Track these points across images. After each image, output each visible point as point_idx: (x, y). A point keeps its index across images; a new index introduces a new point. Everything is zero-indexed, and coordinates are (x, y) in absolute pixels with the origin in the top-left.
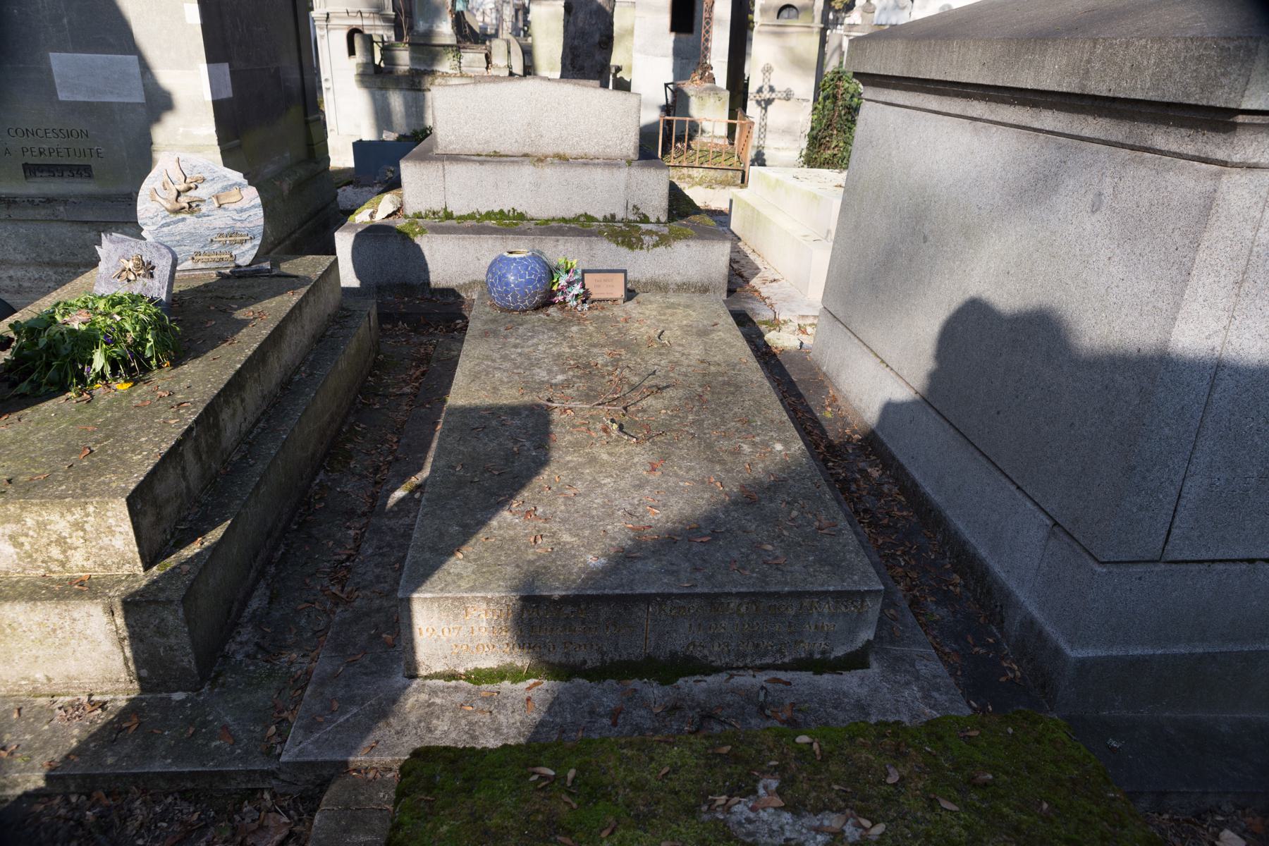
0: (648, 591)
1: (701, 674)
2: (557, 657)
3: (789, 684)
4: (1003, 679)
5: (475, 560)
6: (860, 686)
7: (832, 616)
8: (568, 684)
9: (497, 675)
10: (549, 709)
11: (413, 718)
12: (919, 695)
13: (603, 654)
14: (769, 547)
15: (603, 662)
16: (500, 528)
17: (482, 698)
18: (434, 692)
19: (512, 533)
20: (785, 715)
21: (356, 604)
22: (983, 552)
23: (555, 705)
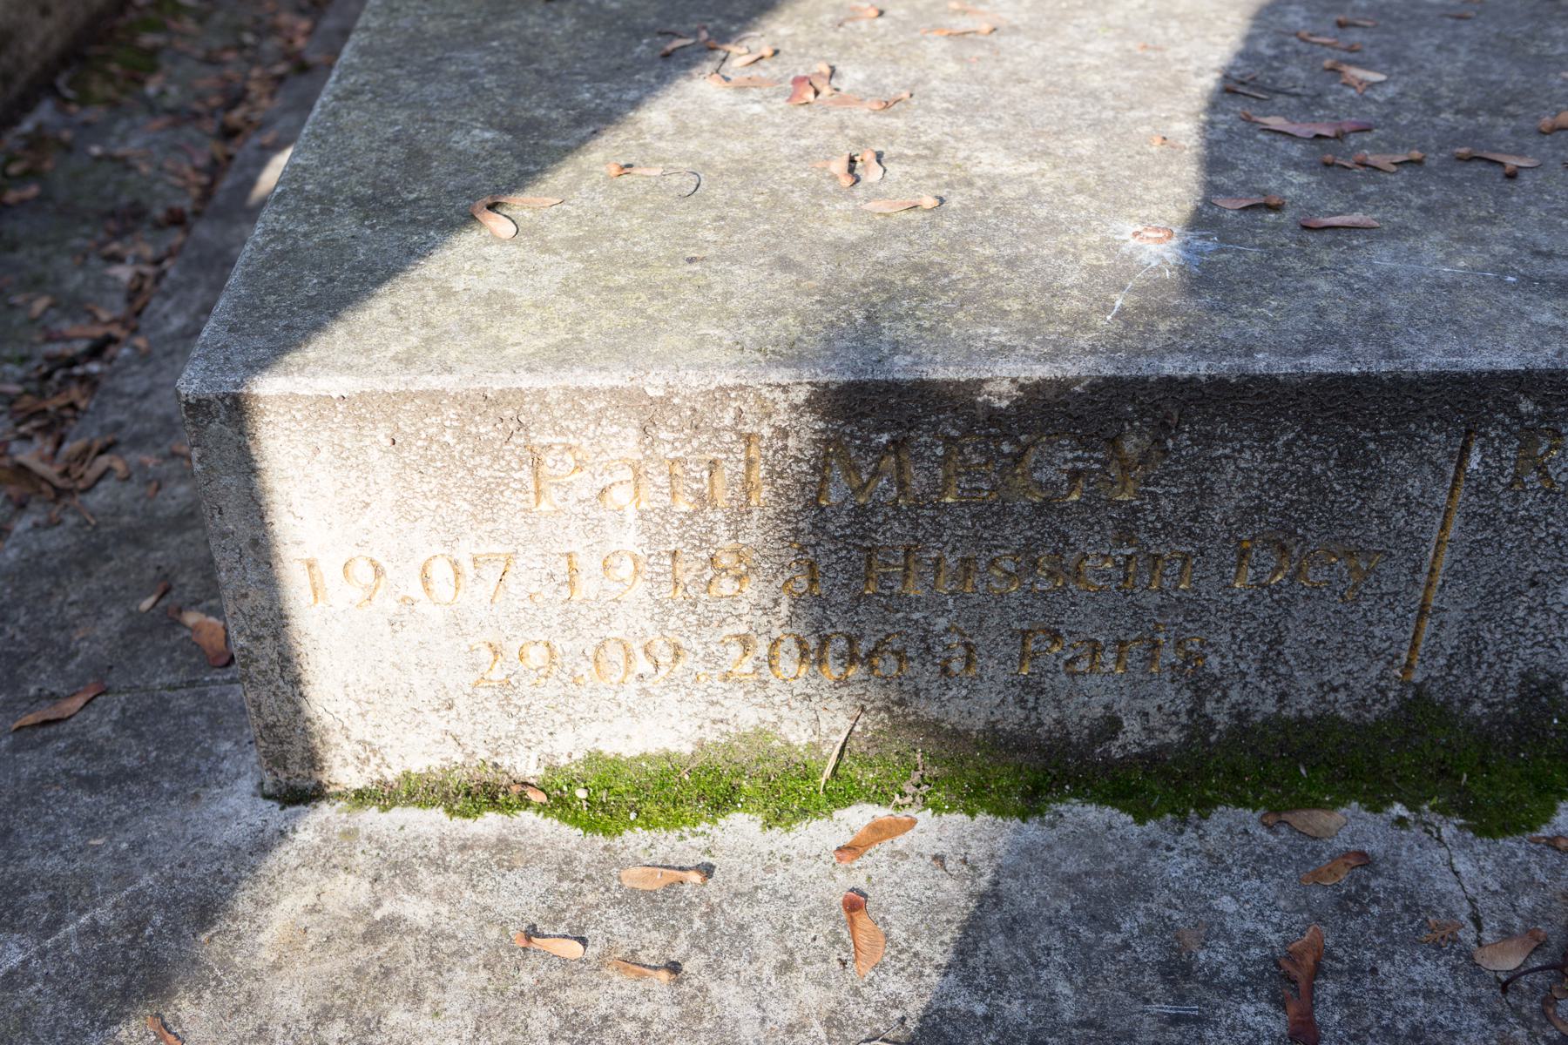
0: (1478, 362)
2: (980, 703)
5: (574, 244)
8: (1033, 830)
9: (709, 788)
10: (963, 952)
11: (289, 999)
15: (1199, 724)
16: (682, 130)
17: (630, 899)
18: (397, 869)
19: (739, 147)
21: (99, 499)
23: (989, 932)
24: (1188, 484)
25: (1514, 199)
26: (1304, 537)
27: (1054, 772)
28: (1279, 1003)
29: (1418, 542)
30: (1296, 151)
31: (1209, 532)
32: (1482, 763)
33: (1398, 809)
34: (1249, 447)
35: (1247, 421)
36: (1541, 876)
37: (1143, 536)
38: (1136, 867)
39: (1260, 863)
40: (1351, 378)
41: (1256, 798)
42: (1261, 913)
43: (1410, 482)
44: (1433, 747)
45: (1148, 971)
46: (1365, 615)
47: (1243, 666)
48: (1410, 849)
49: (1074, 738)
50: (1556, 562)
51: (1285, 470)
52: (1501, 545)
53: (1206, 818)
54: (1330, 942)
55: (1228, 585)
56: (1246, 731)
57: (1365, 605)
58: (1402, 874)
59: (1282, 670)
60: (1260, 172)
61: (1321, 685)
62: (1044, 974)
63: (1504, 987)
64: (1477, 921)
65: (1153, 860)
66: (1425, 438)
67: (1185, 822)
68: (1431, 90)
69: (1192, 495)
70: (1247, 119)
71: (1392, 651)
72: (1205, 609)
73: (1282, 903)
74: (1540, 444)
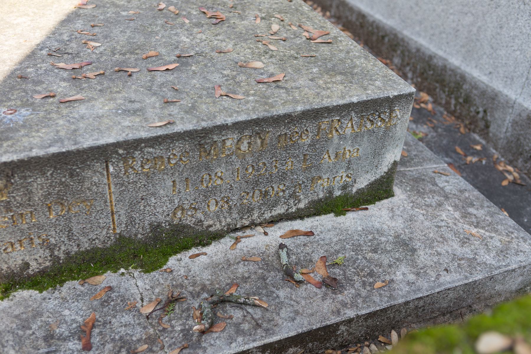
0: (102, 142)
1: (196, 245)
3: (310, 234)
4: (505, 183)
6: (392, 218)
7: (356, 137)
12: (457, 215)
13: (51, 248)
14: (258, 64)
15: (55, 259)
20: (320, 273)
22: (455, 61)
24: (23, 191)
25: (129, 83)
26: (67, 200)
27: (12, 283)
28: (80, 339)
29: (103, 195)
30: (65, 75)
31: (36, 204)
32: (146, 251)
33: (122, 270)
34: (39, 177)
35: (35, 170)
36: (162, 281)
37: (14, 209)
38: (38, 307)
39: (78, 297)
40: (63, 153)
41: (78, 276)
42: (77, 313)
43: (94, 178)
44: (130, 250)
45: (40, 340)
46: (95, 218)
47: (62, 239)
48: (125, 282)
49: (15, 271)
50: (147, 192)
51: (53, 182)
52: (129, 191)
53: (62, 286)
54: (97, 317)
55: (48, 218)
56: (71, 257)
57: (94, 215)
58: (121, 290)
59: (75, 238)
60: (52, 84)
61: (89, 240)
62: (6, 349)
63: (147, 317)
64: (142, 300)
65: (44, 304)
66: (94, 165)
67: (55, 289)
68: (115, 47)
69: (26, 194)
70: (53, 65)
71: (108, 225)
72: (43, 226)
73: (84, 308)
74: (129, 161)
